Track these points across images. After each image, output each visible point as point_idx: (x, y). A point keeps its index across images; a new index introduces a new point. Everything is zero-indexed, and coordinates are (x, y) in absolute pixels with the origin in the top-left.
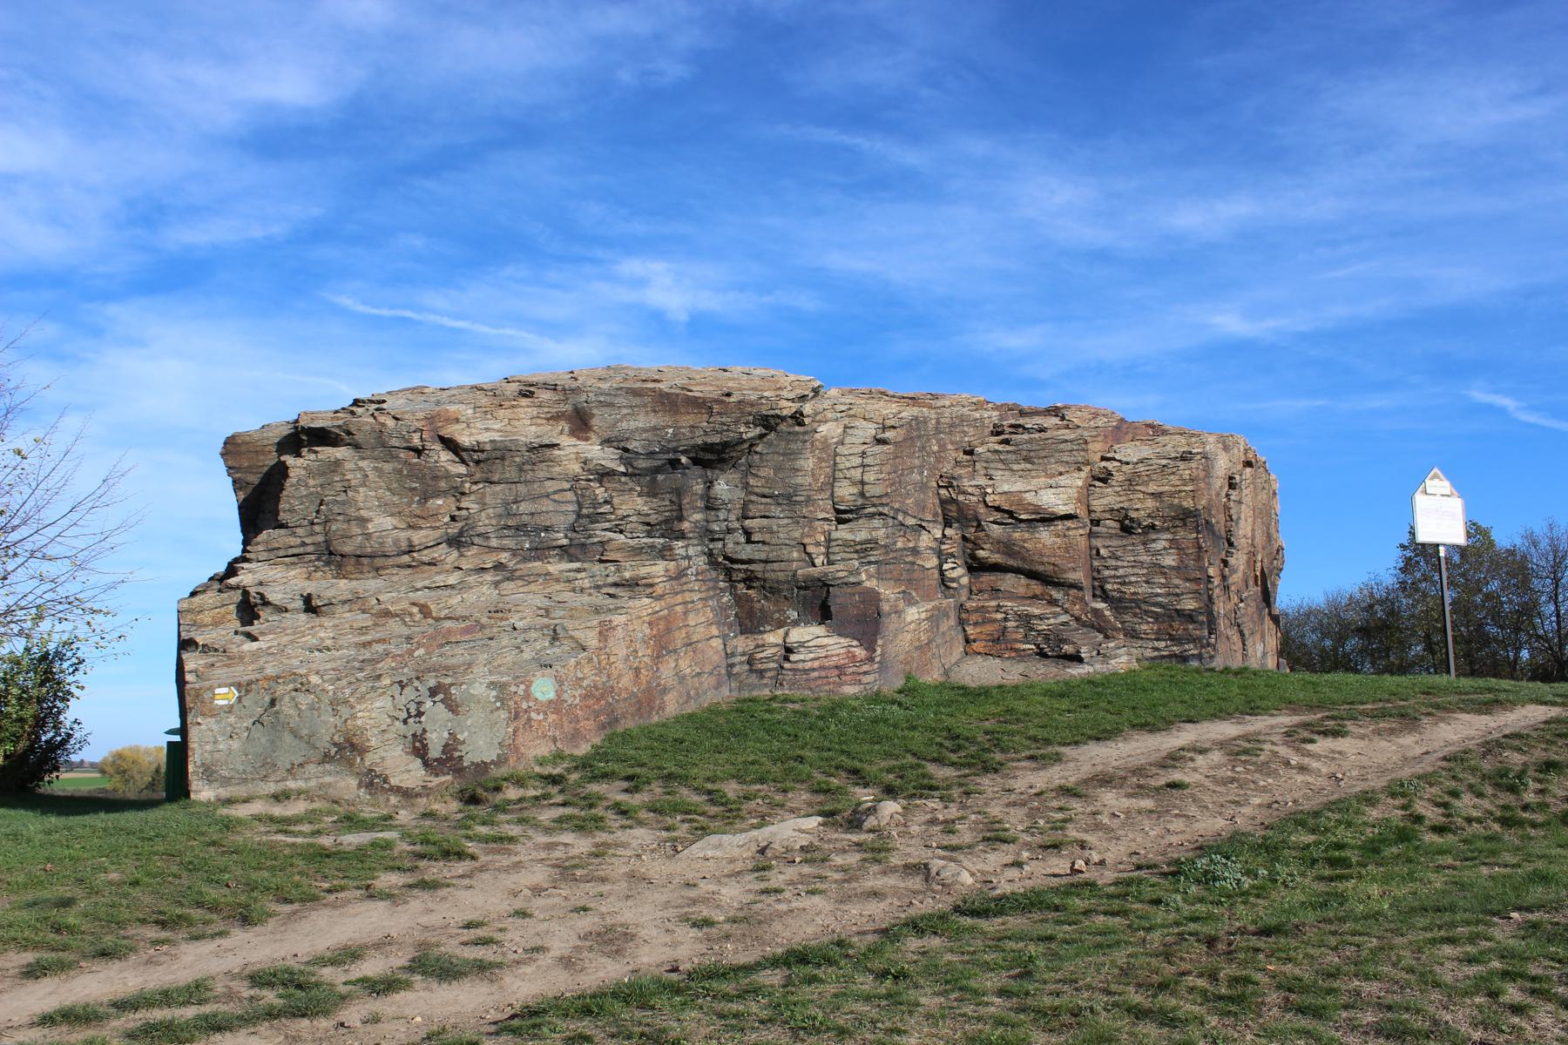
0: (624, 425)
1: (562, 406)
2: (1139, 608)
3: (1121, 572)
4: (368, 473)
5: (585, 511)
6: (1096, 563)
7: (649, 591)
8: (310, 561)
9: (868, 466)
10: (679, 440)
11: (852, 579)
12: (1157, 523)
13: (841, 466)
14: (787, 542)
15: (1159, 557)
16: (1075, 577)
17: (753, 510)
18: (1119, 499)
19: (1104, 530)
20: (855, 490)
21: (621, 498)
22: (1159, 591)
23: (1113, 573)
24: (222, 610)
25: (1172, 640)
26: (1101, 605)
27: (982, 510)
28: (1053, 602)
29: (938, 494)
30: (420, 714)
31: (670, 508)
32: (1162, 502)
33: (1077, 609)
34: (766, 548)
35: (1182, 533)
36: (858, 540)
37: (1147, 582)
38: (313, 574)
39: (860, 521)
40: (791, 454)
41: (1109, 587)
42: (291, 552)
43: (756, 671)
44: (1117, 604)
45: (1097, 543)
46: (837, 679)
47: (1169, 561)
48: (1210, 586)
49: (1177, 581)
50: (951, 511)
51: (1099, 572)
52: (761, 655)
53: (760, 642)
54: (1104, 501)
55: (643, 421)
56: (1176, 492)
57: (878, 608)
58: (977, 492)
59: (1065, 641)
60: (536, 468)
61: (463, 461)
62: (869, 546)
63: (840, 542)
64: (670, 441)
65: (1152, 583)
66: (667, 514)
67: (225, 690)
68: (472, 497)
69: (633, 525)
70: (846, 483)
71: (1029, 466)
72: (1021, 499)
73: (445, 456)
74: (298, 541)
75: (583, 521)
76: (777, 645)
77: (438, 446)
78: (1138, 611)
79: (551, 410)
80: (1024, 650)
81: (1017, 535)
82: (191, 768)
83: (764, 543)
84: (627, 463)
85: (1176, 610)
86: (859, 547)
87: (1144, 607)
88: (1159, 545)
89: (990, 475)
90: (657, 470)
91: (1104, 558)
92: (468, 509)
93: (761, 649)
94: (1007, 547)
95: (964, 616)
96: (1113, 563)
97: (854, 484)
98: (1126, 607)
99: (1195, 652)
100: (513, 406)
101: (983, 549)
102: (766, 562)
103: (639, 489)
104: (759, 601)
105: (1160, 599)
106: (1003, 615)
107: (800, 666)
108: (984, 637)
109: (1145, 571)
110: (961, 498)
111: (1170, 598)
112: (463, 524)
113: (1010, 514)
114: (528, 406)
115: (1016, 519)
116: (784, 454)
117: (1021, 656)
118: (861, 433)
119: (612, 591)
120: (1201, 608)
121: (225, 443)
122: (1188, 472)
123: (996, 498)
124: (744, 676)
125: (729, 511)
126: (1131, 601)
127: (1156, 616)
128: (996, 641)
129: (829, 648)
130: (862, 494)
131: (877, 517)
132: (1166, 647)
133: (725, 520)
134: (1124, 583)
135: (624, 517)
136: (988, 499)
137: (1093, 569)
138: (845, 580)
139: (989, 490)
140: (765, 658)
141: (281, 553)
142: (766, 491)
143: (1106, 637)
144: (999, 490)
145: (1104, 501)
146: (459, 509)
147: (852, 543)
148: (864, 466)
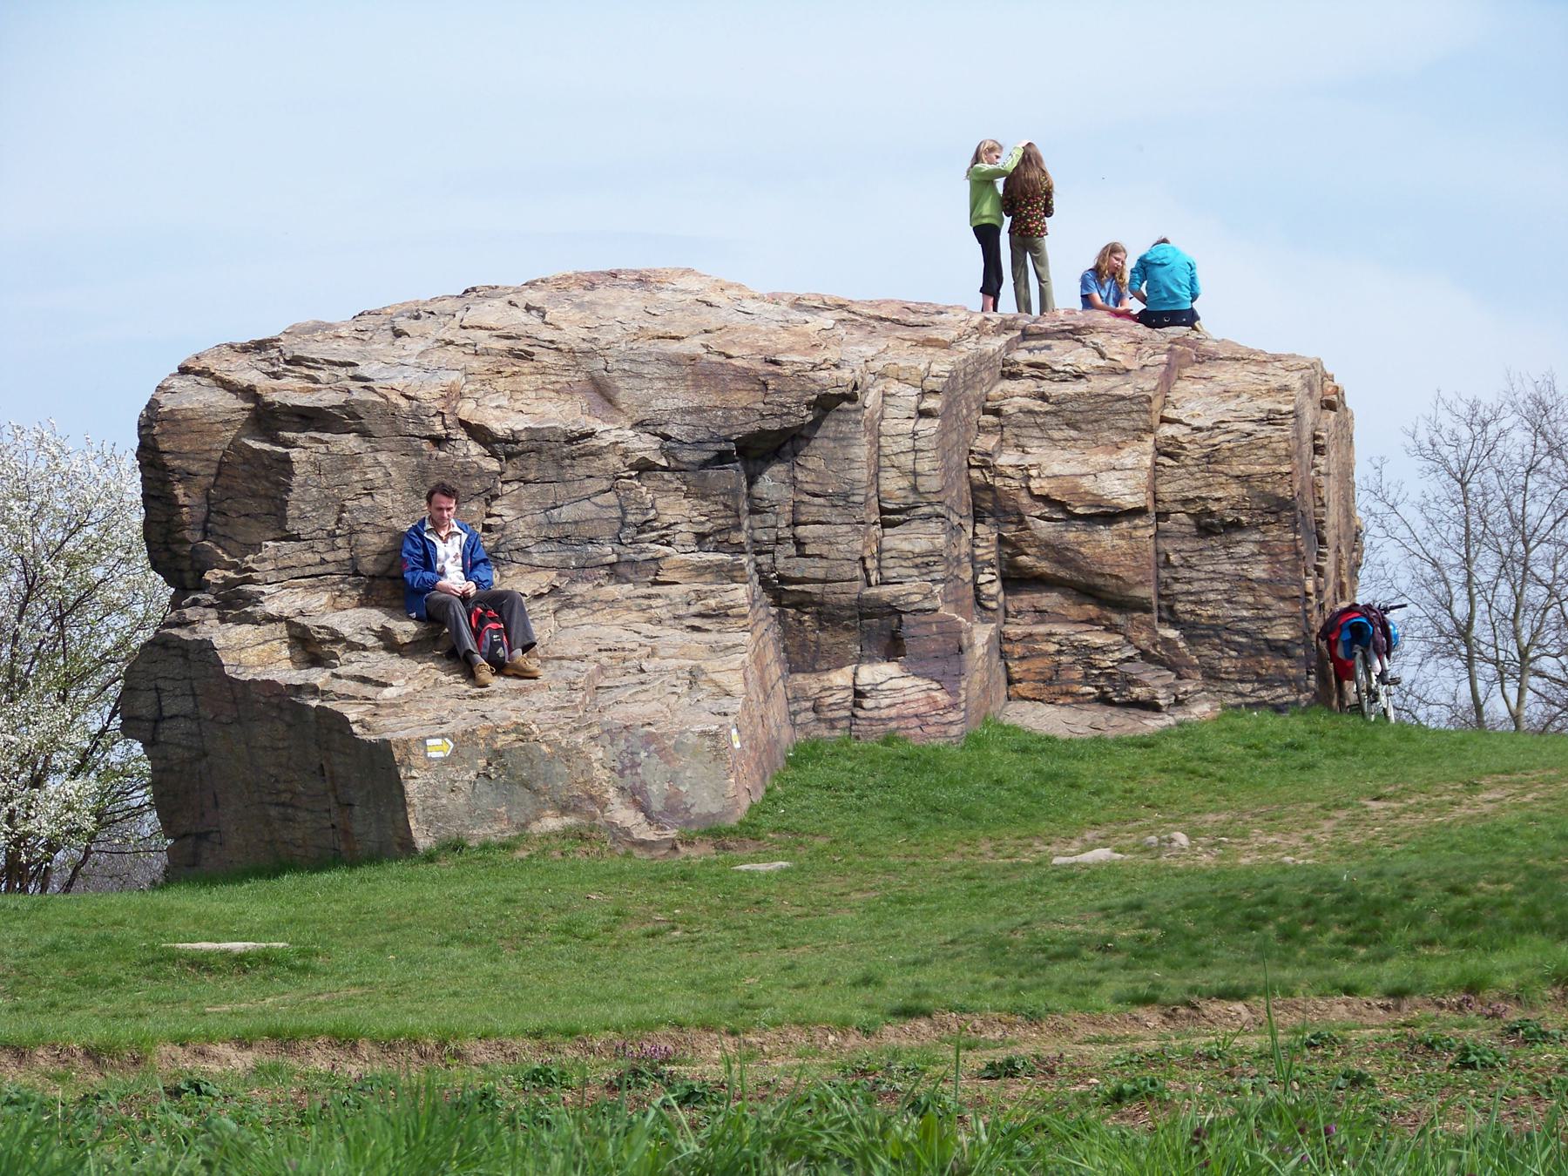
0: (659, 404)
1: (572, 373)
2: (1219, 637)
3: (1195, 587)
4: (390, 470)
5: (630, 518)
6: (1164, 574)
7: (742, 622)
8: (334, 584)
9: (922, 451)
10: (732, 426)
11: (927, 605)
12: (1243, 518)
13: (887, 451)
14: (849, 556)
15: (1245, 567)
16: (1143, 595)
17: (806, 513)
18: (1194, 484)
19: (1175, 527)
20: (904, 483)
21: (665, 500)
22: (1245, 613)
23: (1186, 587)
24: (266, 647)
25: (1261, 682)
26: (1172, 633)
27: (1025, 500)
28: (1111, 629)
29: (969, 477)
30: (635, 765)
31: (724, 514)
32: (1250, 487)
33: (1143, 639)
34: (824, 563)
35: (1275, 532)
36: (917, 550)
37: (1229, 601)
38: (338, 600)
39: (914, 525)
40: (843, 439)
41: (1179, 607)
42: (308, 571)
43: (825, 720)
44: (1192, 632)
45: (1166, 545)
46: (918, 730)
47: (1259, 571)
48: (1308, 607)
49: (1268, 600)
50: (984, 500)
51: (1167, 586)
52: (831, 700)
53: (827, 684)
54: (1174, 486)
55: (682, 398)
56: (1268, 475)
57: (959, 640)
58: (1018, 475)
59: (1135, 683)
60: (575, 463)
61: (494, 455)
62: (932, 559)
63: (893, 553)
64: (720, 427)
65: (1236, 602)
66: (720, 521)
67: (439, 741)
68: (505, 501)
69: (684, 536)
70: (893, 473)
71: (1073, 433)
72: (1076, 486)
73: (475, 449)
74: (317, 558)
75: (631, 531)
76: (846, 688)
77: (461, 435)
78: (1217, 641)
79: (558, 379)
80: (1083, 695)
81: (1070, 536)
82: (412, 824)
83: (821, 556)
84: (666, 453)
85: (1266, 640)
86: (919, 561)
87: (1225, 635)
88: (1246, 549)
89: (1023, 447)
90: (705, 464)
91: (1175, 567)
92: (501, 516)
93: (828, 693)
94: (1055, 551)
95: (1007, 647)
96: (1187, 574)
97: (904, 474)
98: (1203, 636)
99: (1292, 698)
100: (514, 374)
101: (1027, 555)
102: (824, 581)
103: (685, 488)
104: (814, 631)
105: (1245, 625)
106: (1057, 647)
107: (875, 714)
108: (1031, 676)
109: (1226, 586)
110: (998, 483)
111: (1259, 624)
112: (499, 535)
113: (1061, 506)
114: (531, 374)
115: (1069, 513)
116: (835, 439)
117: (1079, 700)
118: (904, 404)
119: (697, 622)
120: (1298, 638)
121: (140, 428)
122: (1283, 445)
123: (1044, 484)
124: (811, 727)
125: (777, 514)
126: (1210, 627)
127: (1239, 648)
128: (1049, 682)
129: (906, 692)
130: (914, 488)
131: (934, 519)
132: (1253, 691)
133: (774, 527)
134: (1199, 603)
135: (671, 525)
136: (1033, 484)
137: (1160, 582)
138: (919, 606)
139: (1033, 472)
140: (835, 704)
141: (296, 573)
142: (816, 489)
143: (1179, 677)
144: (1047, 472)
145: (1174, 486)
146: (489, 516)
147: (910, 555)
148: (916, 451)
